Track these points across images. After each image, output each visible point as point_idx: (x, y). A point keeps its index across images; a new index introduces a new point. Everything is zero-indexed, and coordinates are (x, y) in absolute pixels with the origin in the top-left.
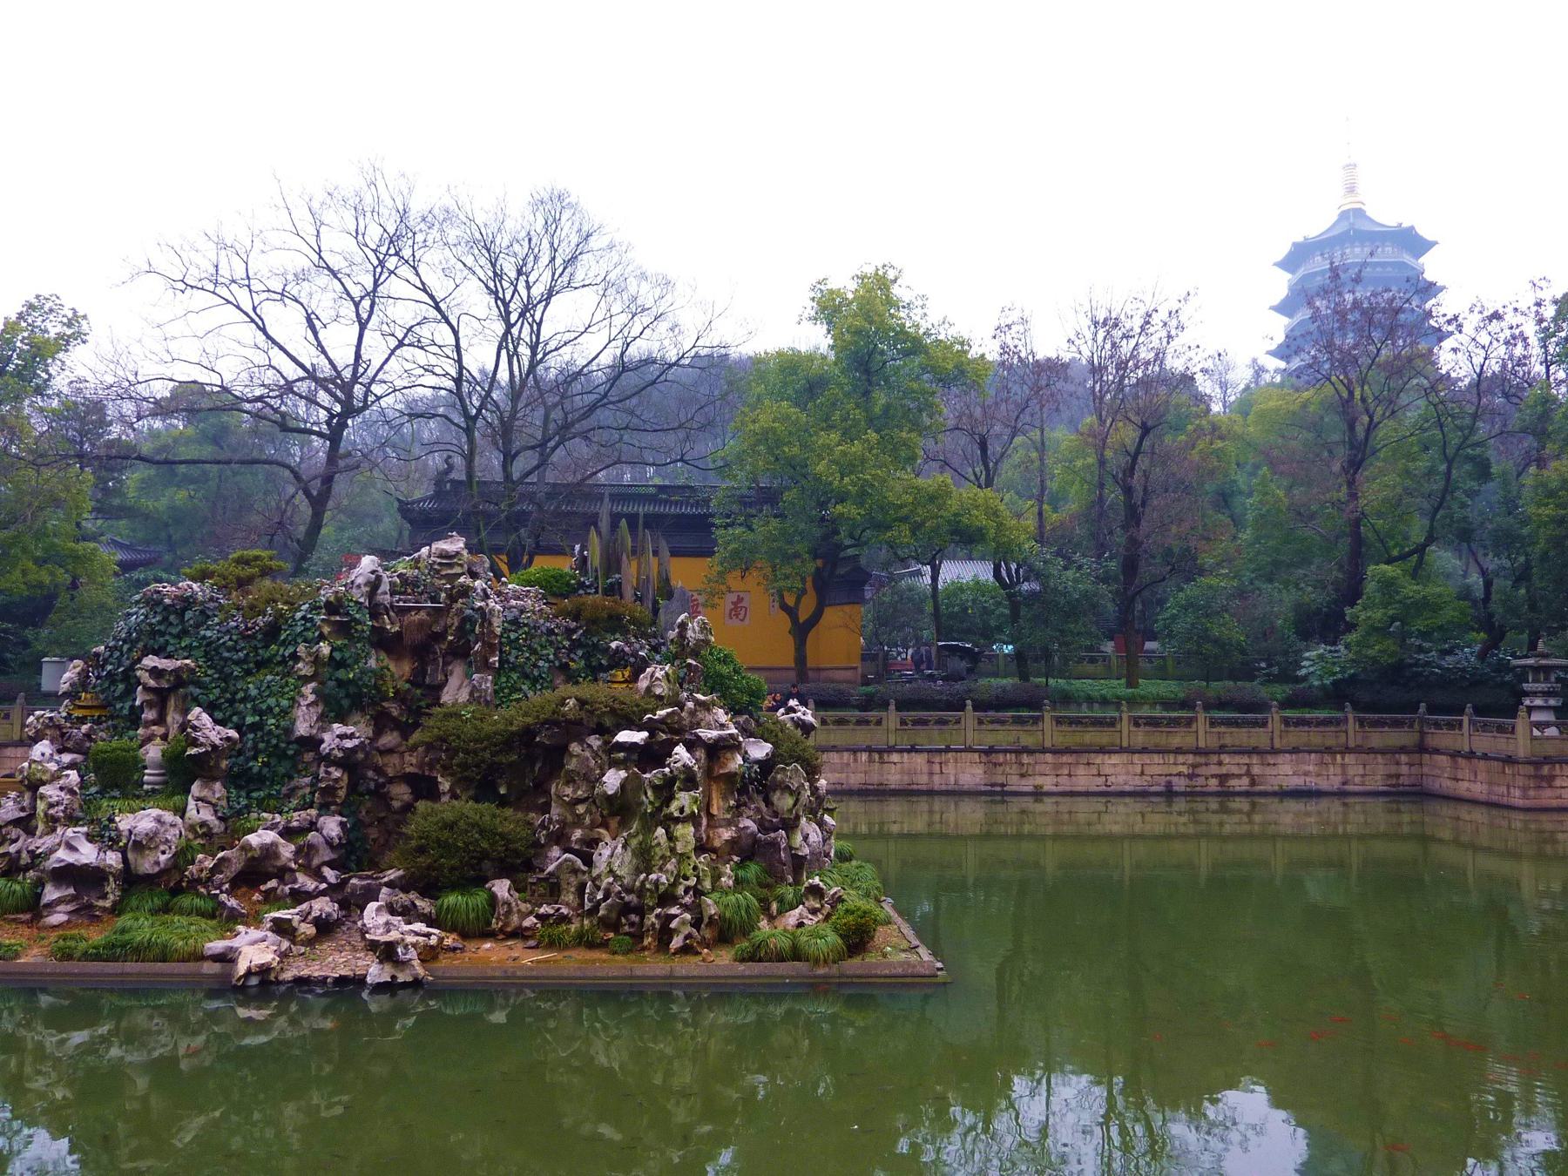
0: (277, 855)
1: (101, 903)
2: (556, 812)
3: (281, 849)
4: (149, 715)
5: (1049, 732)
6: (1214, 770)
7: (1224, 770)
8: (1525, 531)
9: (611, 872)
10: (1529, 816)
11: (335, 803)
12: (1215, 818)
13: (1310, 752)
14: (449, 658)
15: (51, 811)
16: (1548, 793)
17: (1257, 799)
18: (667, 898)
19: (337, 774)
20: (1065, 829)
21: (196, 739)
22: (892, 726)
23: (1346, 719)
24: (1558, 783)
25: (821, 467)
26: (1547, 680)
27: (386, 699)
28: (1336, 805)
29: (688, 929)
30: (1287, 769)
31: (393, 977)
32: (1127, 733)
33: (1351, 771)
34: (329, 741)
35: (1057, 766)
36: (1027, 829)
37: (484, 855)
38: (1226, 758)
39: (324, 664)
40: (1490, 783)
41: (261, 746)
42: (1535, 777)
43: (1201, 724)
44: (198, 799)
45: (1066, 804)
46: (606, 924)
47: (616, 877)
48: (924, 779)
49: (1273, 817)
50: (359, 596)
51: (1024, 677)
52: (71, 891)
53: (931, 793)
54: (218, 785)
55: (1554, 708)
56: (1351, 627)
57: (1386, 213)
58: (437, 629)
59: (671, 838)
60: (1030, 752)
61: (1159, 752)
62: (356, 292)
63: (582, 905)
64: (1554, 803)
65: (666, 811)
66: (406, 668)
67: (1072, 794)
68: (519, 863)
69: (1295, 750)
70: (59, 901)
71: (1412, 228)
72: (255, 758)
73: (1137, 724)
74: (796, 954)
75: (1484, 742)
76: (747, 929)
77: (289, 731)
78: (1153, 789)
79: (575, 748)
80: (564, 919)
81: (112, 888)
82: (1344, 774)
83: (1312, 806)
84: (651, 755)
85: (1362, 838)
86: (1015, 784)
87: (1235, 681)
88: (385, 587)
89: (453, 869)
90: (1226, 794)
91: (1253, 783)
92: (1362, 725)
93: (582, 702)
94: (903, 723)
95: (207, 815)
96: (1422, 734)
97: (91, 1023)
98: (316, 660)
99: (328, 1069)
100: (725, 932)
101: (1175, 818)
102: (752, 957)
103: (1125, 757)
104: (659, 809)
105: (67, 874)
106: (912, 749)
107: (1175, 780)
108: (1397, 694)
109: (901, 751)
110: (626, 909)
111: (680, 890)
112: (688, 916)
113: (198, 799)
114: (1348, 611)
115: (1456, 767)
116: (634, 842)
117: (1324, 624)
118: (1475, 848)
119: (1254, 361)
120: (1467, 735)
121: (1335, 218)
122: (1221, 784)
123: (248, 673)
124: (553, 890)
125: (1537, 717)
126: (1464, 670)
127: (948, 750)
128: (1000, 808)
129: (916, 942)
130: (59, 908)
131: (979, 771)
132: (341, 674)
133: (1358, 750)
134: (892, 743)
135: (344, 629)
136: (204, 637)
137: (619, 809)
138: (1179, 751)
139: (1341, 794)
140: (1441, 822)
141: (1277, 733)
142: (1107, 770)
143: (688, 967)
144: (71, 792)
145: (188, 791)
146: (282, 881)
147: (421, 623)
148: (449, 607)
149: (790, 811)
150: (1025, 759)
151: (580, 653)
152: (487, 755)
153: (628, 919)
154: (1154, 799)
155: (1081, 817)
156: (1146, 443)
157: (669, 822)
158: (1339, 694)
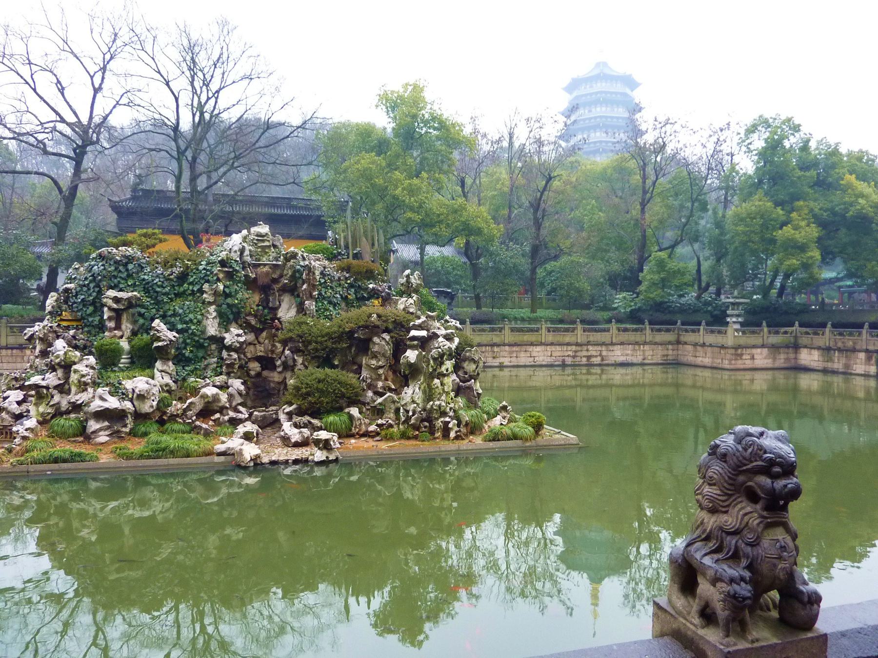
0: (219, 400)
1: (124, 429)
2: (365, 373)
3: (221, 397)
4: (112, 324)
5: (508, 336)
6: (585, 353)
9: (413, 402)
11: (233, 372)
12: (584, 377)
14: (281, 293)
15: (83, 379)
16: (740, 362)
18: (444, 414)
19: (235, 356)
20: (514, 384)
21: (159, 337)
24: (744, 357)
25: (398, 191)
26: (738, 309)
27: (250, 314)
28: (639, 370)
29: (456, 429)
30: (618, 353)
31: (327, 457)
33: (647, 353)
34: (229, 339)
35: (511, 352)
37: (343, 396)
38: (590, 348)
39: (220, 295)
41: (188, 341)
43: (579, 331)
44: (162, 371)
45: (515, 371)
46: (416, 427)
47: (418, 404)
49: (612, 376)
50: (236, 256)
51: (479, 307)
52: (106, 423)
54: (170, 363)
55: (741, 323)
58: (275, 276)
59: (442, 384)
60: (498, 345)
62: (93, 69)
64: (742, 367)
66: (257, 298)
68: (354, 401)
69: (622, 344)
70: (101, 429)
71: (630, 75)
72: (185, 348)
73: (549, 331)
75: (710, 339)
77: (203, 332)
78: (557, 363)
79: (376, 339)
80: (391, 426)
81: (129, 420)
82: (644, 355)
83: (629, 370)
86: (491, 362)
87: (576, 309)
88: (247, 253)
90: (590, 365)
91: (602, 360)
93: (379, 316)
95: (167, 380)
96: (679, 335)
97: (124, 496)
98: (216, 293)
100: (473, 429)
101: (566, 377)
103: (543, 347)
105: (101, 415)
107: (566, 358)
108: (659, 316)
110: (423, 420)
113: (162, 371)
115: (696, 351)
116: (422, 387)
118: (703, 388)
120: (703, 335)
122: (588, 360)
123: (172, 300)
124: (379, 412)
126: (690, 305)
130: (101, 433)
132: (229, 300)
135: (230, 276)
136: (144, 280)
138: (568, 344)
139: (642, 364)
140: (687, 376)
142: (534, 354)
143: (464, 444)
144: (92, 368)
145: (154, 367)
147: (267, 273)
148: (284, 265)
149: (474, 371)
150: (496, 349)
151: (353, 290)
152: (329, 344)
153: (427, 424)
157: (441, 376)
158: (635, 317)
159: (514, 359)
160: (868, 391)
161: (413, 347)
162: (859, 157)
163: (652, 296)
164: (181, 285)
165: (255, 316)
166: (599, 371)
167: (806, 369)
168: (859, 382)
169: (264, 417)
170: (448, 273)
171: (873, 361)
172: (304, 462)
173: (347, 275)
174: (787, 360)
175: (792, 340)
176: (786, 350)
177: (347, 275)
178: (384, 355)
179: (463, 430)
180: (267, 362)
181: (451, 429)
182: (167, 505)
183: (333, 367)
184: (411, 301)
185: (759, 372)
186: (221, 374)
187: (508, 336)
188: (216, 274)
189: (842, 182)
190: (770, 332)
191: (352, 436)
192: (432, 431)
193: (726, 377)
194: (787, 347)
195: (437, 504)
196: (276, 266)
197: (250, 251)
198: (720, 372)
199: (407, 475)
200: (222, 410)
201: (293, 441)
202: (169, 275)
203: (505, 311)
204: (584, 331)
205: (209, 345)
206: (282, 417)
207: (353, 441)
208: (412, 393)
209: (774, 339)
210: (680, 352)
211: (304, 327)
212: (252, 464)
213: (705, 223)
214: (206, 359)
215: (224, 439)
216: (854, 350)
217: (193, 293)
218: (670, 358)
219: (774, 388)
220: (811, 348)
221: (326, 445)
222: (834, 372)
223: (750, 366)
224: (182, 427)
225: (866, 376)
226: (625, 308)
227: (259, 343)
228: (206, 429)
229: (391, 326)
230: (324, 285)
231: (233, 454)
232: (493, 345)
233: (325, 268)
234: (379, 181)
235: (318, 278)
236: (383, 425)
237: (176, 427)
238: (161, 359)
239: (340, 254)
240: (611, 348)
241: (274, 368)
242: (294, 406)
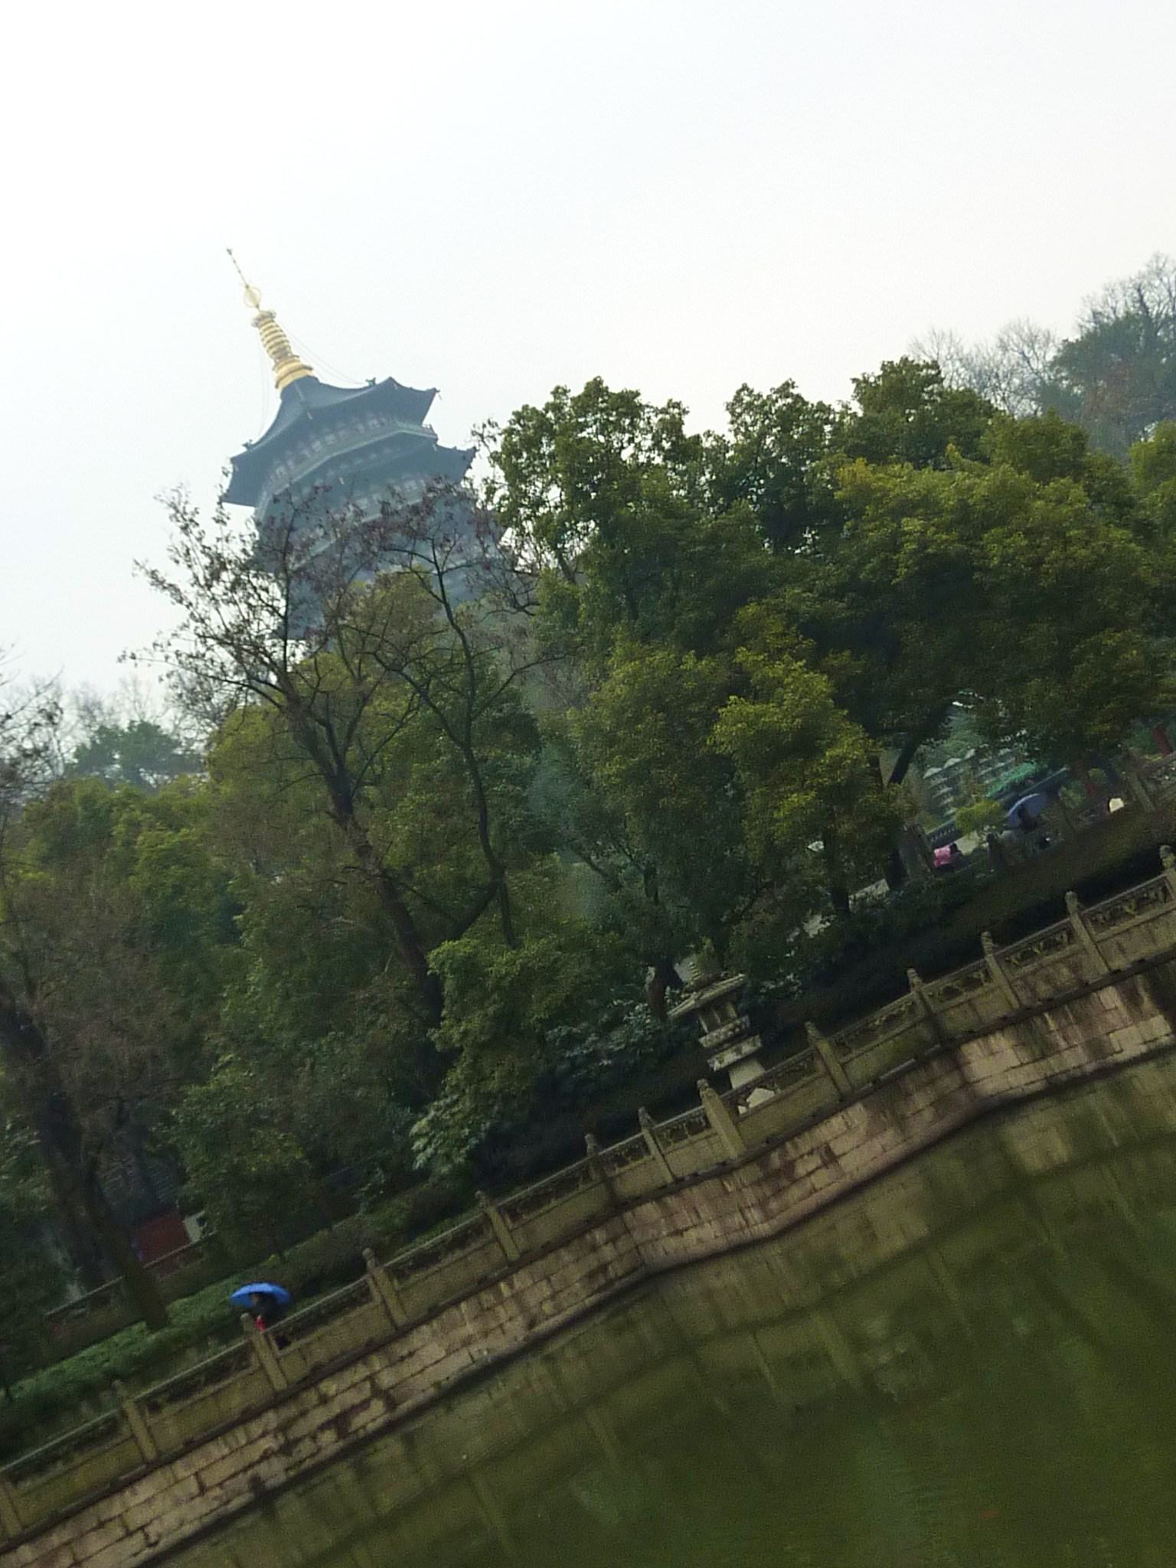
6: (320, 1416)
7: (336, 1409)
10: (788, 1243)
13: (456, 1303)
16: (795, 1192)
17: (412, 1427)
23: (487, 1220)
24: (801, 1170)
26: (725, 1018)
28: (536, 1369)
30: (433, 1351)
33: (532, 1300)
38: (330, 1387)
40: (720, 1217)
43: (265, 1354)
56: (449, 1057)
57: (346, 370)
61: (212, 1438)
64: (812, 1202)
69: (433, 1313)
73: (155, 1408)
75: (684, 1158)
78: (236, 1503)
82: (523, 1309)
83: (501, 1389)
90: (357, 1448)
91: (391, 1404)
92: (515, 1216)
96: (608, 1182)
103: (160, 1478)
107: (262, 1470)
115: (669, 1214)
117: (418, 1075)
118: (752, 1327)
121: (277, 403)
122: (342, 1433)
126: (642, 1043)
133: (527, 1259)
138: (249, 1415)
139: (535, 1345)
141: (392, 1303)
142: (136, 1519)
154: (245, 1522)
158: (492, 1169)
162: (899, 387)
167: (1011, 1106)
171: (1147, 1004)
174: (941, 1103)
175: (925, 1032)
176: (922, 1076)
185: (875, 1191)
190: (841, 1046)
204: (283, 1343)
209: (864, 1064)
210: (637, 1236)
216: (1086, 991)
219: (950, 1217)
220: (981, 1032)
223: (835, 1188)
226: (448, 1157)
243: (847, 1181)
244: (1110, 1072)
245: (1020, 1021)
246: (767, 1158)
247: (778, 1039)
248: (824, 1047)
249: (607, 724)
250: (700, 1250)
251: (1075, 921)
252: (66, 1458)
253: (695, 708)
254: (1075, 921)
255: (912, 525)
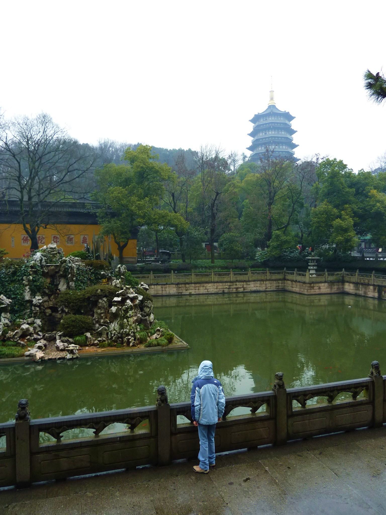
2: (96, 316)
5: (193, 278)
6: (235, 286)
8: (311, 223)
9: (114, 330)
10: (308, 296)
12: (235, 299)
16: (313, 290)
18: (128, 335)
19: (38, 309)
22: (152, 278)
24: (315, 288)
25: (133, 208)
26: (314, 262)
27: (45, 288)
28: (264, 294)
29: (133, 341)
30: (252, 286)
32: (215, 278)
33: (268, 285)
34: (35, 301)
36: (187, 304)
37: (83, 328)
40: (300, 288)
41: (17, 303)
42: (310, 287)
46: (115, 341)
47: (116, 331)
48: (160, 292)
53: (162, 296)
54: (8, 314)
57: (282, 107)
58: (57, 270)
59: (128, 321)
60: (188, 284)
63: (108, 337)
64: (314, 293)
65: (126, 315)
66: (48, 280)
67: (199, 294)
68: (90, 329)
69: (254, 281)
71: (289, 113)
74: (158, 345)
75: (299, 278)
76: (146, 340)
77: (24, 298)
79: (100, 301)
80: (104, 341)
82: (266, 286)
83: (259, 295)
84: (123, 302)
85: (270, 302)
86: (185, 292)
87: (237, 261)
88: (43, 261)
89: (76, 331)
90: (237, 293)
91: (244, 289)
93: (102, 290)
94: (155, 277)
96: (285, 275)
98: (29, 281)
99: (39, 379)
100: (141, 341)
102: (150, 345)
103: (212, 284)
104: (125, 315)
106: (157, 284)
107: (225, 289)
109: (154, 285)
111: (130, 333)
112: (133, 338)
113: (4, 317)
114: (268, 243)
115: (292, 284)
116: (119, 323)
118: (296, 304)
119: (243, 154)
120: (295, 277)
122: (236, 290)
123: (9, 284)
124: (100, 334)
125: (311, 272)
127: (167, 284)
128: (180, 299)
129: (181, 340)
131: (175, 289)
132: (35, 283)
133: (270, 280)
134: (152, 283)
135: (35, 272)
137: (115, 316)
138: (226, 282)
139: (265, 291)
140: (289, 298)
142: (207, 288)
143: (135, 349)
146: (31, 336)
147: (53, 269)
150: (187, 286)
153: (120, 340)
154: (220, 295)
155: (201, 300)
156: (218, 197)
157: (127, 318)
159: (197, 291)
160: (374, 306)
161: (115, 305)
163: (273, 254)
164: (13, 277)
165: (48, 289)
166: (242, 296)
167: (348, 294)
168: (371, 301)
169: (50, 336)
170: (172, 240)
171: (376, 291)
172: (63, 358)
173: (91, 268)
175: (341, 278)
176: (338, 284)
177: (91, 268)
178: (104, 308)
179: (137, 342)
180: (54, 309)
181: (131, 342)
182: (8, 376)
183: (82, 314)
184: (118, 281)
185: (323, 296)
186: (31, 317)
187: (193, 278)
188: (29, 272)
189: (369, 194)
190: (329, 275)
191: (87, 346)
192: (122, 343)
193: (306, 298)
194: (338, 282)
195: (126, 374)
196: (57, 266)
197: (45, 259)
198: (303, 296)
199: (112, 362)
200: (31, 335)
201: (60, 348)
202: (8, 272)
203: (199, 262)
205: (26, 304)
206: (57, 337)
207: (87, 348)
208: (115, 326)
209: (331, 278)
210: (285, 284)
211: (68, 296)
212: (40, 360)
213: (302, 216)
214: (25, 310)
215: (29, 349)
216: (369, 285)
217: (19, 280)
218: (280, 287)
219: (331, 303)
220: (350, 282)
221: (71, 352)
222: (360, 296)
224: (12, 343)
225: (373, 298)
227: (50, 300)
228: (23, 344)
229: (107, 294)
230: (78, 274)
231: (33, 356)
232: (186, 284)
233: (79, 266)
234: (124, 202)
235: (75, 272)
236: (100, 340)
237: (10, 343)
238: (4, 312)
239: (89, 256)
240: (248, 283)
241: (57, 312)
242: (62, 333)
243: (320, 293)
244: (365, 297)
245: (356, 284)
246: (312, 284)
247: (320, 269)
248: (326, 273)
249: (318, 213)
250: (294, 291)
251: (372, 275)
252: (203, 276)
253: (332, 217)
254: (372, 275)
255: (378, 204)
